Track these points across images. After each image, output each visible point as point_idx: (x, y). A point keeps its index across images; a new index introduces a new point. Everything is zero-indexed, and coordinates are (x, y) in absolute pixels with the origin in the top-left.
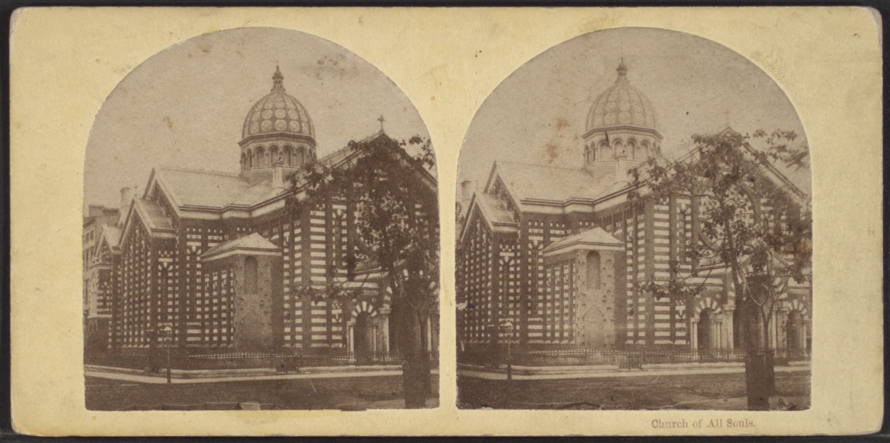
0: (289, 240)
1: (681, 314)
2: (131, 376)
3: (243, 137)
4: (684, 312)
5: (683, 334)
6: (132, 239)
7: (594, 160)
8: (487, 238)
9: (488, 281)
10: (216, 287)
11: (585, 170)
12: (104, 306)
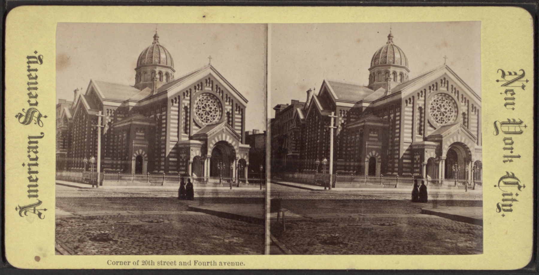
0: (159, 118)
1: (183, 158)
2: (301, 186)
3: (371, 66)
4: (419, 159)
5: (183, 168)
6: (79, 115)
7: (141, 81)
8: (86, 117)
9: (85, 138)
10: (358, 141)
11: (370, 87)
12: (64, 148)
